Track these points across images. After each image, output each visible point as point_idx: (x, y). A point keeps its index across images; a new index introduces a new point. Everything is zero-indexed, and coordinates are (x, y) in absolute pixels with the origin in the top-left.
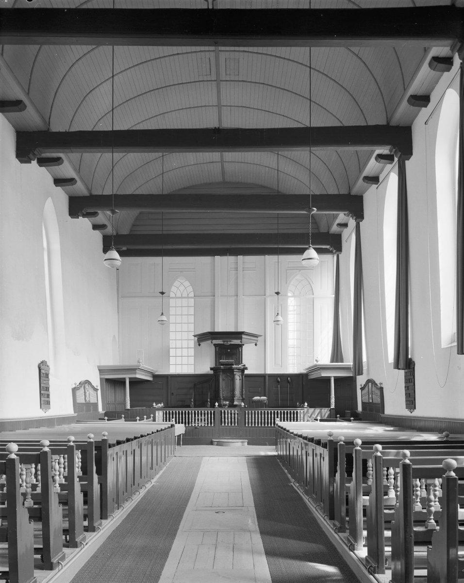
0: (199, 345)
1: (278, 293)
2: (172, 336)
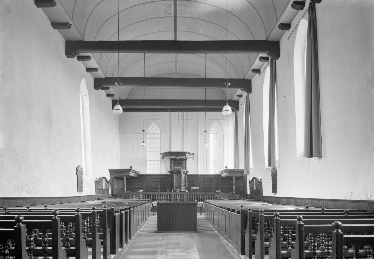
0: (163, 159)
1: (205, 132)
2: (148, 154)
